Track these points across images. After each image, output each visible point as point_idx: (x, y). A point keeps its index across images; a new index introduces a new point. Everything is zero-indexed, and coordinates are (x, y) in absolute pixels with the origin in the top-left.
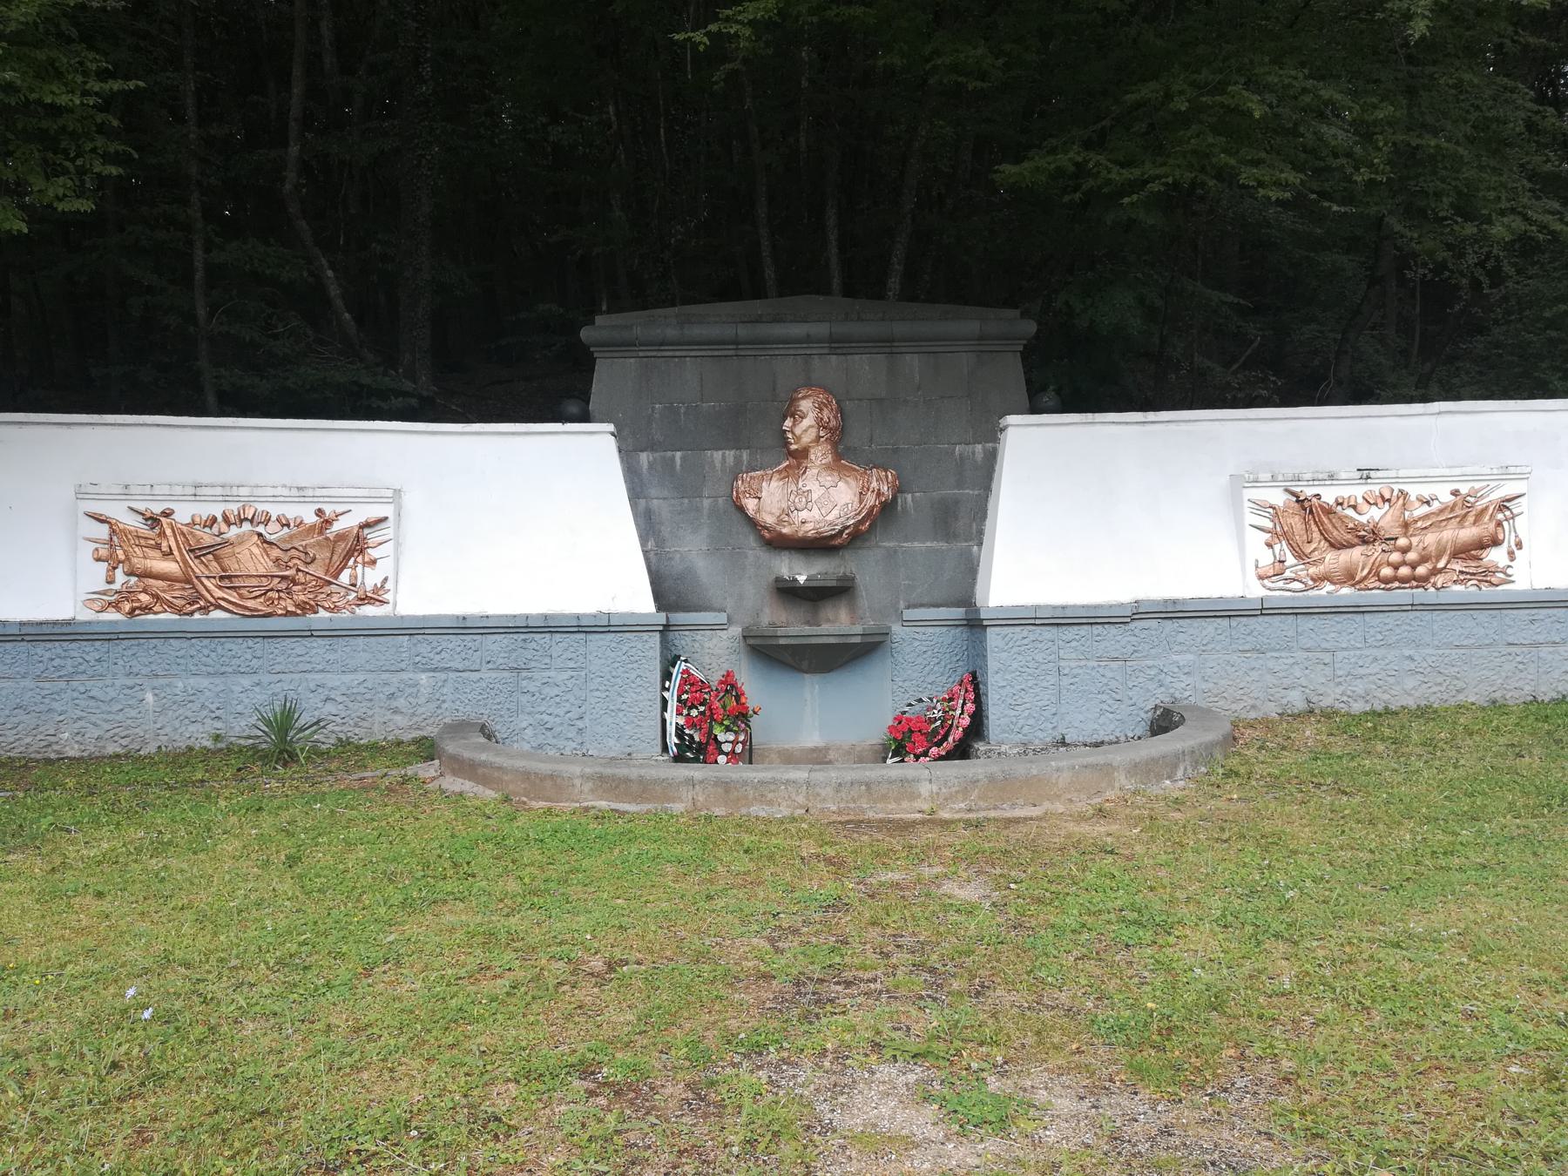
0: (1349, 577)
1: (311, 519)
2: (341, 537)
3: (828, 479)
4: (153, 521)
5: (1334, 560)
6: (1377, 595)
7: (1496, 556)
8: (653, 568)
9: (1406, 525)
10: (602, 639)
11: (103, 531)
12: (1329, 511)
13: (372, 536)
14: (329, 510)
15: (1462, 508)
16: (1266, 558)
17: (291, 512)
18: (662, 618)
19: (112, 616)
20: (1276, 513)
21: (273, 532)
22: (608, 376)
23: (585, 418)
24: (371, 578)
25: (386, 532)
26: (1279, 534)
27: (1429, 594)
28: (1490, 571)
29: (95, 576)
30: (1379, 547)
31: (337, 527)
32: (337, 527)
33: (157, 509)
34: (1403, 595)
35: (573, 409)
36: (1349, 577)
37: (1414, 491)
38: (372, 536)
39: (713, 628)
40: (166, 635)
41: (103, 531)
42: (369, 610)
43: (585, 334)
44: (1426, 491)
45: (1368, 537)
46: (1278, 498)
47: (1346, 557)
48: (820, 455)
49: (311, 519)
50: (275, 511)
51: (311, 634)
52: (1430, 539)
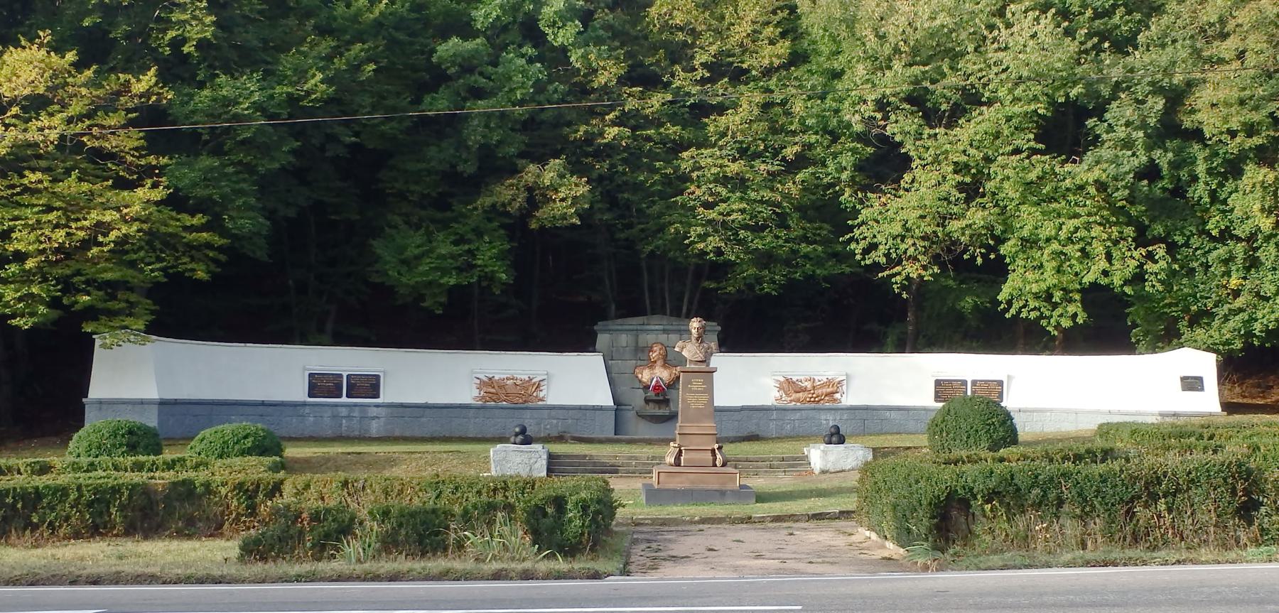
0: (798, 400)
1: (527, 379)
2: (535, 384)
3: (662, 370)
4: (490, 379)
5: (795, 396)
6: (807, 405)
7: (837, 396)
8: (775, 603)
9: (814, 387)
10: (823, 555)
11: (478, 381)
12: (794, 383)
13: (542, 383)
14: (531, 377)
15: (829, 383)
16: (778, 395)
17: (523, 377)
18: (616, 407)
19: (480, 403)
20: (781, 383)
21: (519, 382)
22: (603, 339)
23: (594, 351)
24: (542, 394)
25: (545, 382)
26: (780, 388)
27: (820, 405)
28: (835, 400)
29: (476, 393)
30: (806, 393)
31: (534, 381)
32: (534, 381)
33: (491, 376)
34: (813, 405)
35: (591, 349)
36: (798, 400)
37: (816, 378)
38: (542, 383)
39: (628, 410)
40: (492, 408)
41: (478, 381)
42: (540, 403)
43: (595, 328)
44: (820, 378)
45: (804, 390)
46: (782, 379)
47: (798, 395)
48: (659, 363)
49: (527, 379)
50: (519, 377)
51: (527, 408)
52: (820, 391)
